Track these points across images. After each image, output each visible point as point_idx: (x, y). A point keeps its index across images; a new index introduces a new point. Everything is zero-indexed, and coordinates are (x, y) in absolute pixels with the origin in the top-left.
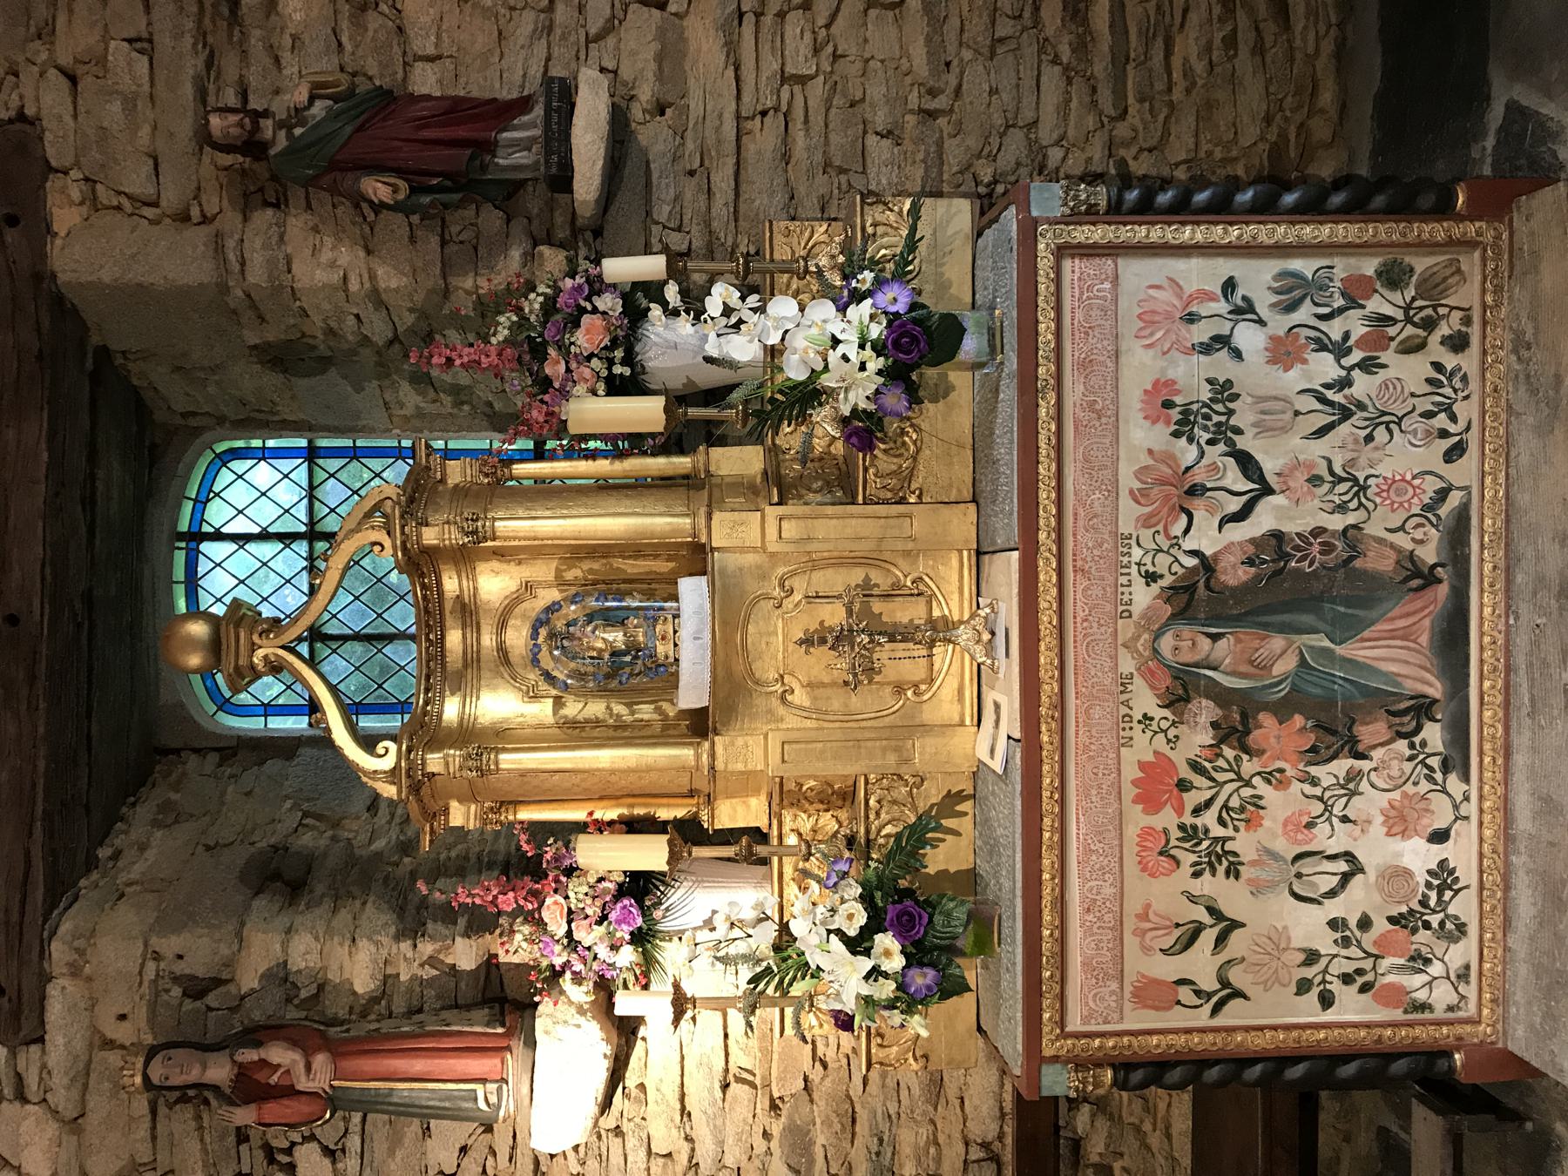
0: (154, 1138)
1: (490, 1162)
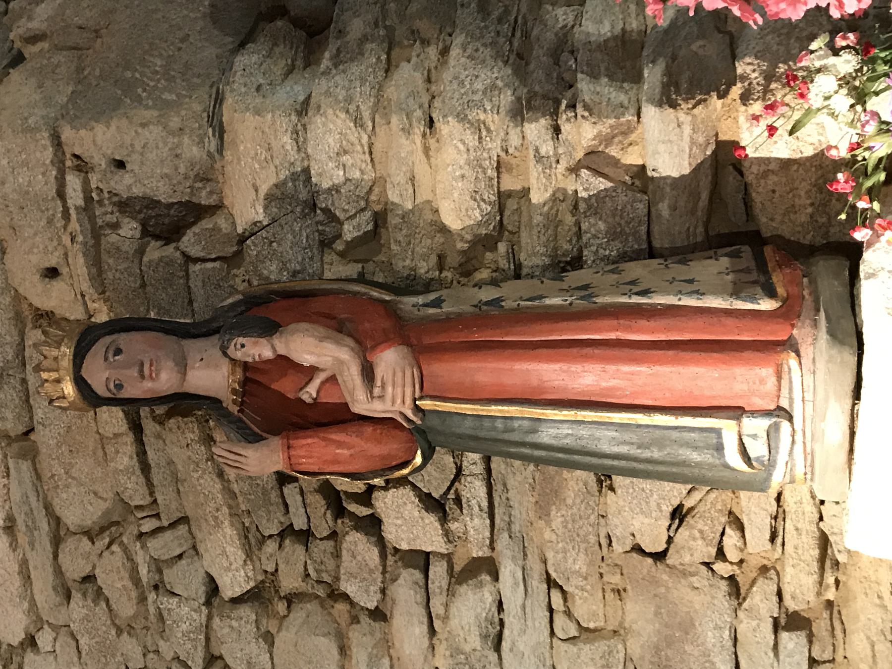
0: (145, 468)
1: (731, 540)
